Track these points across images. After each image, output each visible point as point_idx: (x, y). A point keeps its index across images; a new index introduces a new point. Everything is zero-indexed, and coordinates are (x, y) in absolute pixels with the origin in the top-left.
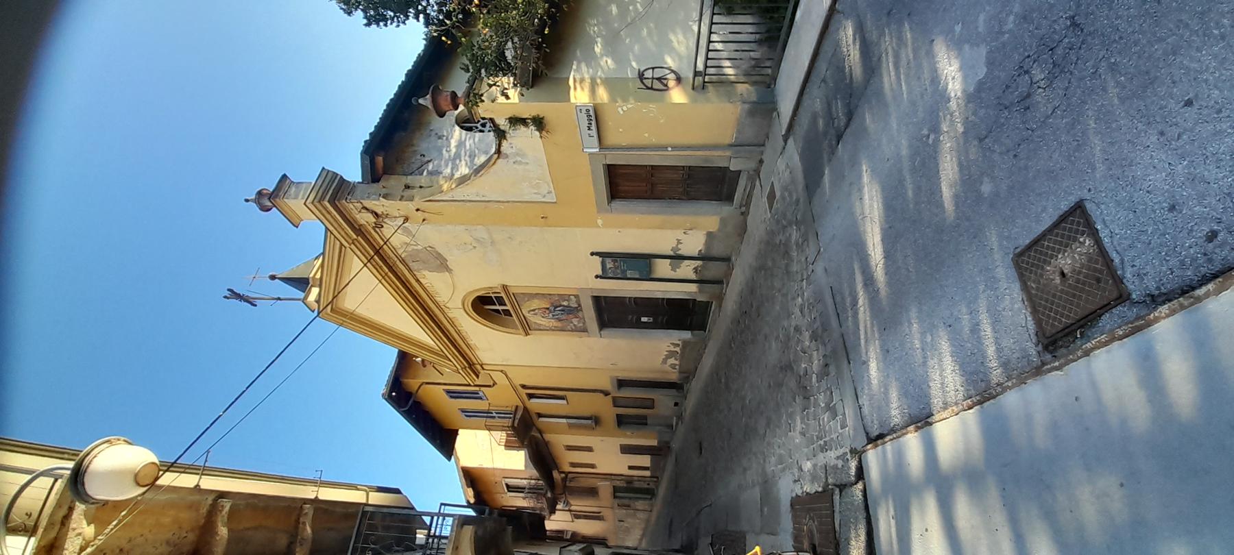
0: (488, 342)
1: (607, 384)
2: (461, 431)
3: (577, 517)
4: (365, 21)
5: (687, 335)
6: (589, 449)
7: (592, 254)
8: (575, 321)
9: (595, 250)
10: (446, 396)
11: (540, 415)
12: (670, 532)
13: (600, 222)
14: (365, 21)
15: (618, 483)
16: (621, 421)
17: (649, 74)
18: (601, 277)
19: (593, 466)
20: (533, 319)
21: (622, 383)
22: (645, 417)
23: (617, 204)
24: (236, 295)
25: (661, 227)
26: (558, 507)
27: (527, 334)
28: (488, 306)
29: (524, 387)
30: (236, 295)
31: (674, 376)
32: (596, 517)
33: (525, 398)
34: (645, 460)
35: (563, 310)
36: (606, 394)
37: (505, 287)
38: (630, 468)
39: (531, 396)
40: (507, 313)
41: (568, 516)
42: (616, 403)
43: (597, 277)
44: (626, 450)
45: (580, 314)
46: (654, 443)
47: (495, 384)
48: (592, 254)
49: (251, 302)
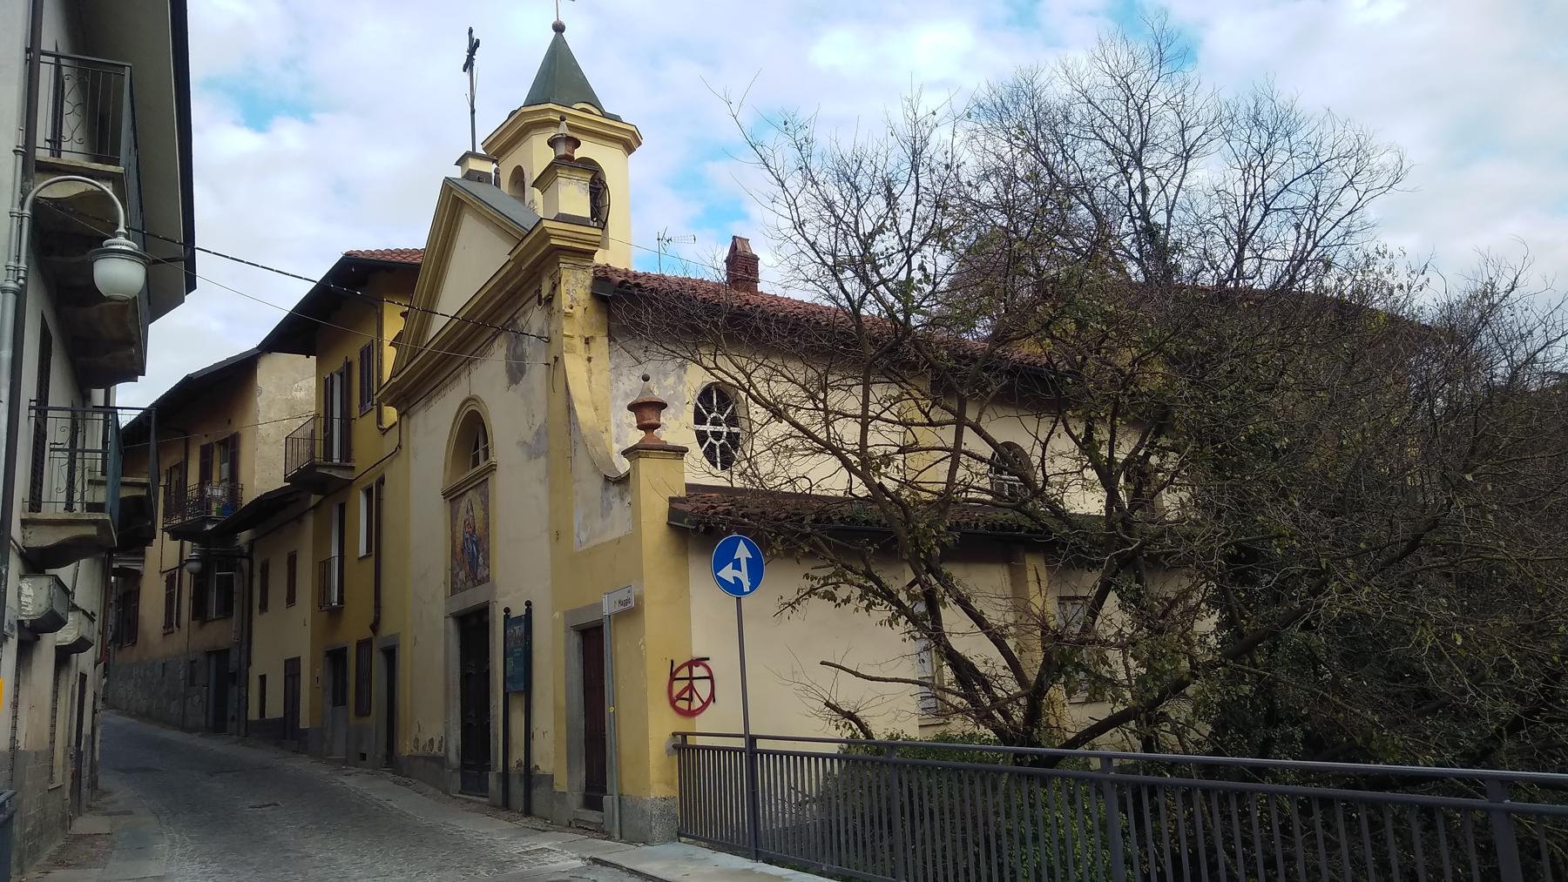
0: (436, 423)
1: (387, 628)
2: (313, 358)
3: (170, 582)
4: (529, 437)
5: (454, 758)
6: (291, 600)
7: (528, 604)
8: (462, 575)
9: (534, 607)
10: (366, 342)
11: (342, 508)
12: (834, 708)
13: (557, 615)
14: (529, 437)
15: (234, 657)
16: (336, 658)
17: (699, 671)
18: (507, 617)
19: (264, 607)
20: (464, 504)
21: (391, 654)
22: (344, 702)
23: (576, 640)
24: (474, 46)
25: (556, 708)
26: (188, 544)
27: (446, 495)
28: (472, 433)
29: (381, 481)
30: (474, 46)
31: (405, 747)
32: (170, 624)
33: (367, 484)
34: (275, 709)
35: (471, 555)
36: (375, 627)
37: (492, 468)
38: (263, 678)
39: (369, 492)
40: (476, 463)
41: (171, 561)
42: (364, 645)
43: (507, 610)
44: (292, 667)
45: (470, 583)
46: (304, 723)
47: (384, 432)
48: (528, 604)
49: (469, 65)
